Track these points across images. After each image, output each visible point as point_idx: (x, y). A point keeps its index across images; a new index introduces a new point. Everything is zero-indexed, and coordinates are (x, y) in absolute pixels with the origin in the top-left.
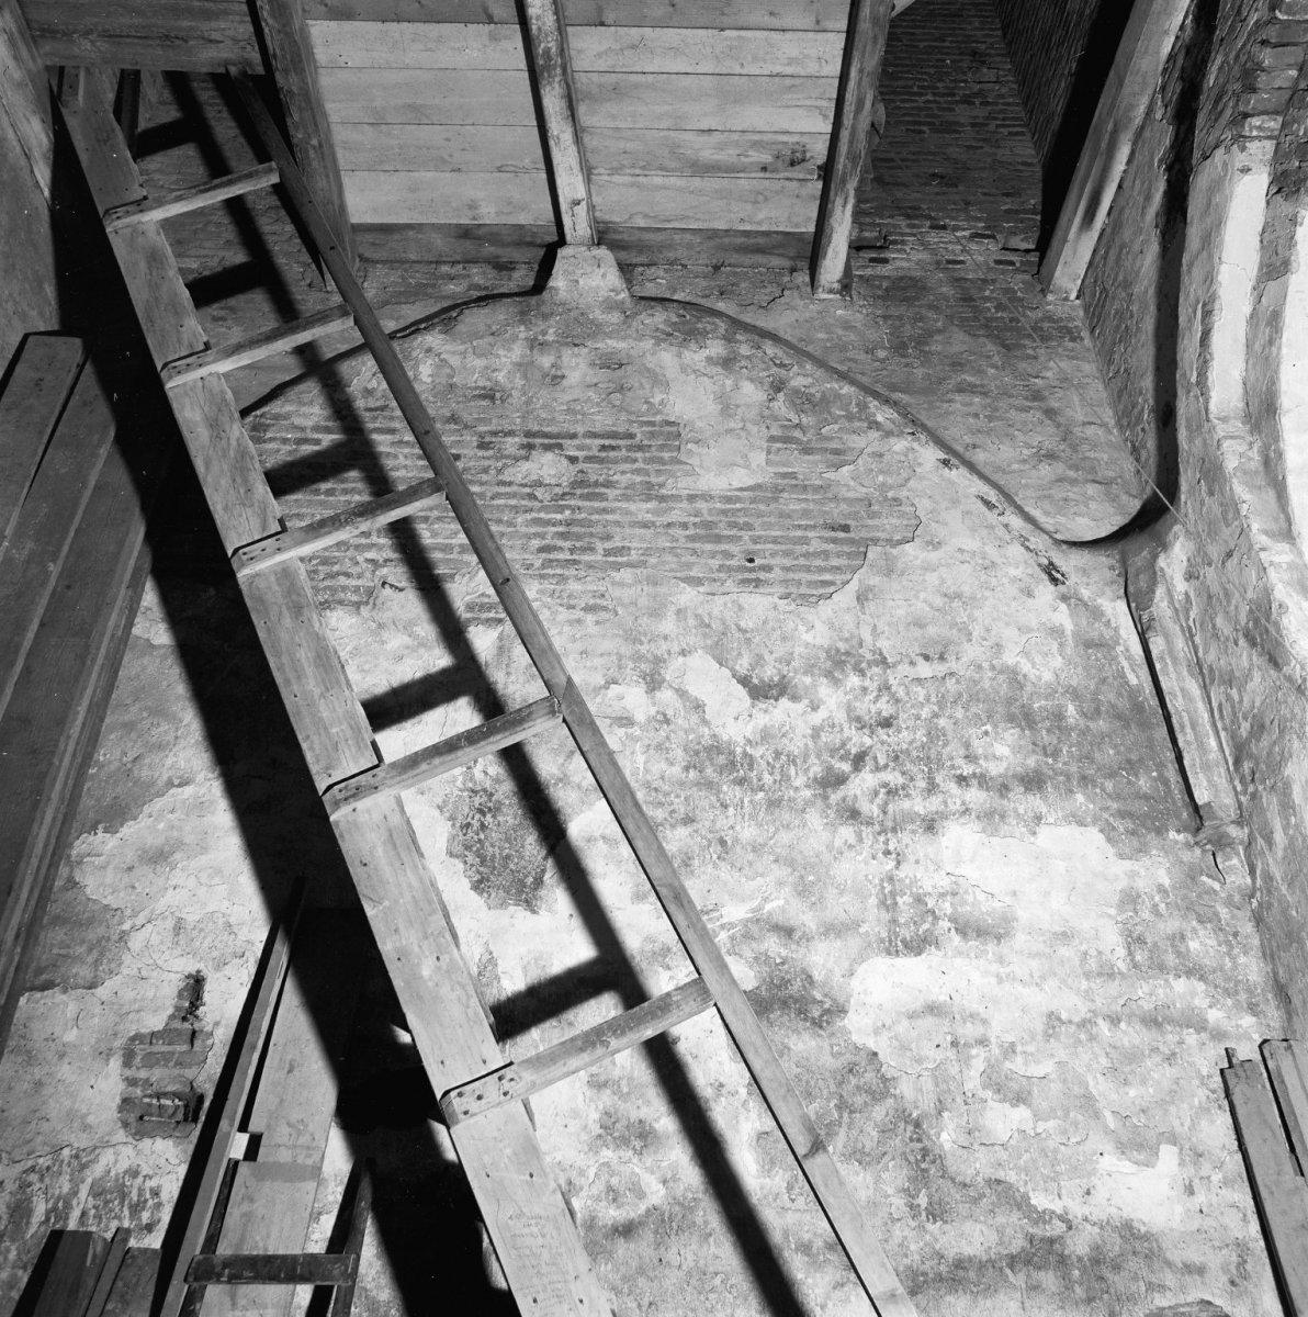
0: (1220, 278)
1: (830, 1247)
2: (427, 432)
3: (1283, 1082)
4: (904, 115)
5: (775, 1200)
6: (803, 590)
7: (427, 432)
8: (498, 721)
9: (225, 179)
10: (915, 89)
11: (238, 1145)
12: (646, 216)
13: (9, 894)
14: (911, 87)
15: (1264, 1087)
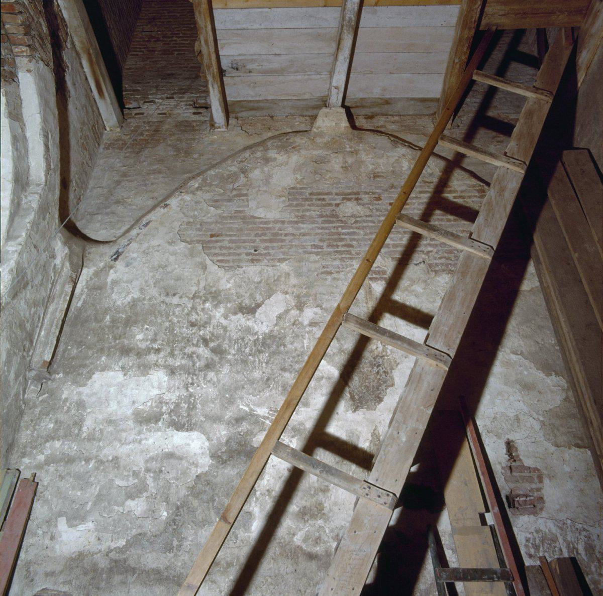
0: (456, 19)
1: (218, 564)
2: (404, 193)
3: (10, 488)
4: (183, 47)
5: (243, 543)
6: (231, 264)
7: (404, 193)
8: (371, 324)
9: (501, 79)
10: (181, 35)
11: (490, 518)
12: (331, 73)
13: (595, 401)
14: (179, 34)
15: (19, 490)
